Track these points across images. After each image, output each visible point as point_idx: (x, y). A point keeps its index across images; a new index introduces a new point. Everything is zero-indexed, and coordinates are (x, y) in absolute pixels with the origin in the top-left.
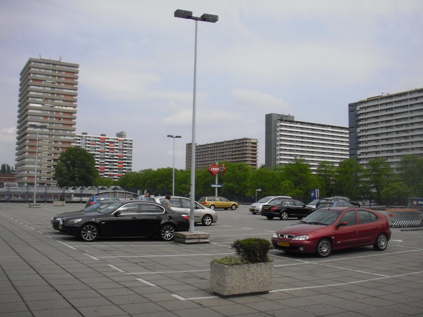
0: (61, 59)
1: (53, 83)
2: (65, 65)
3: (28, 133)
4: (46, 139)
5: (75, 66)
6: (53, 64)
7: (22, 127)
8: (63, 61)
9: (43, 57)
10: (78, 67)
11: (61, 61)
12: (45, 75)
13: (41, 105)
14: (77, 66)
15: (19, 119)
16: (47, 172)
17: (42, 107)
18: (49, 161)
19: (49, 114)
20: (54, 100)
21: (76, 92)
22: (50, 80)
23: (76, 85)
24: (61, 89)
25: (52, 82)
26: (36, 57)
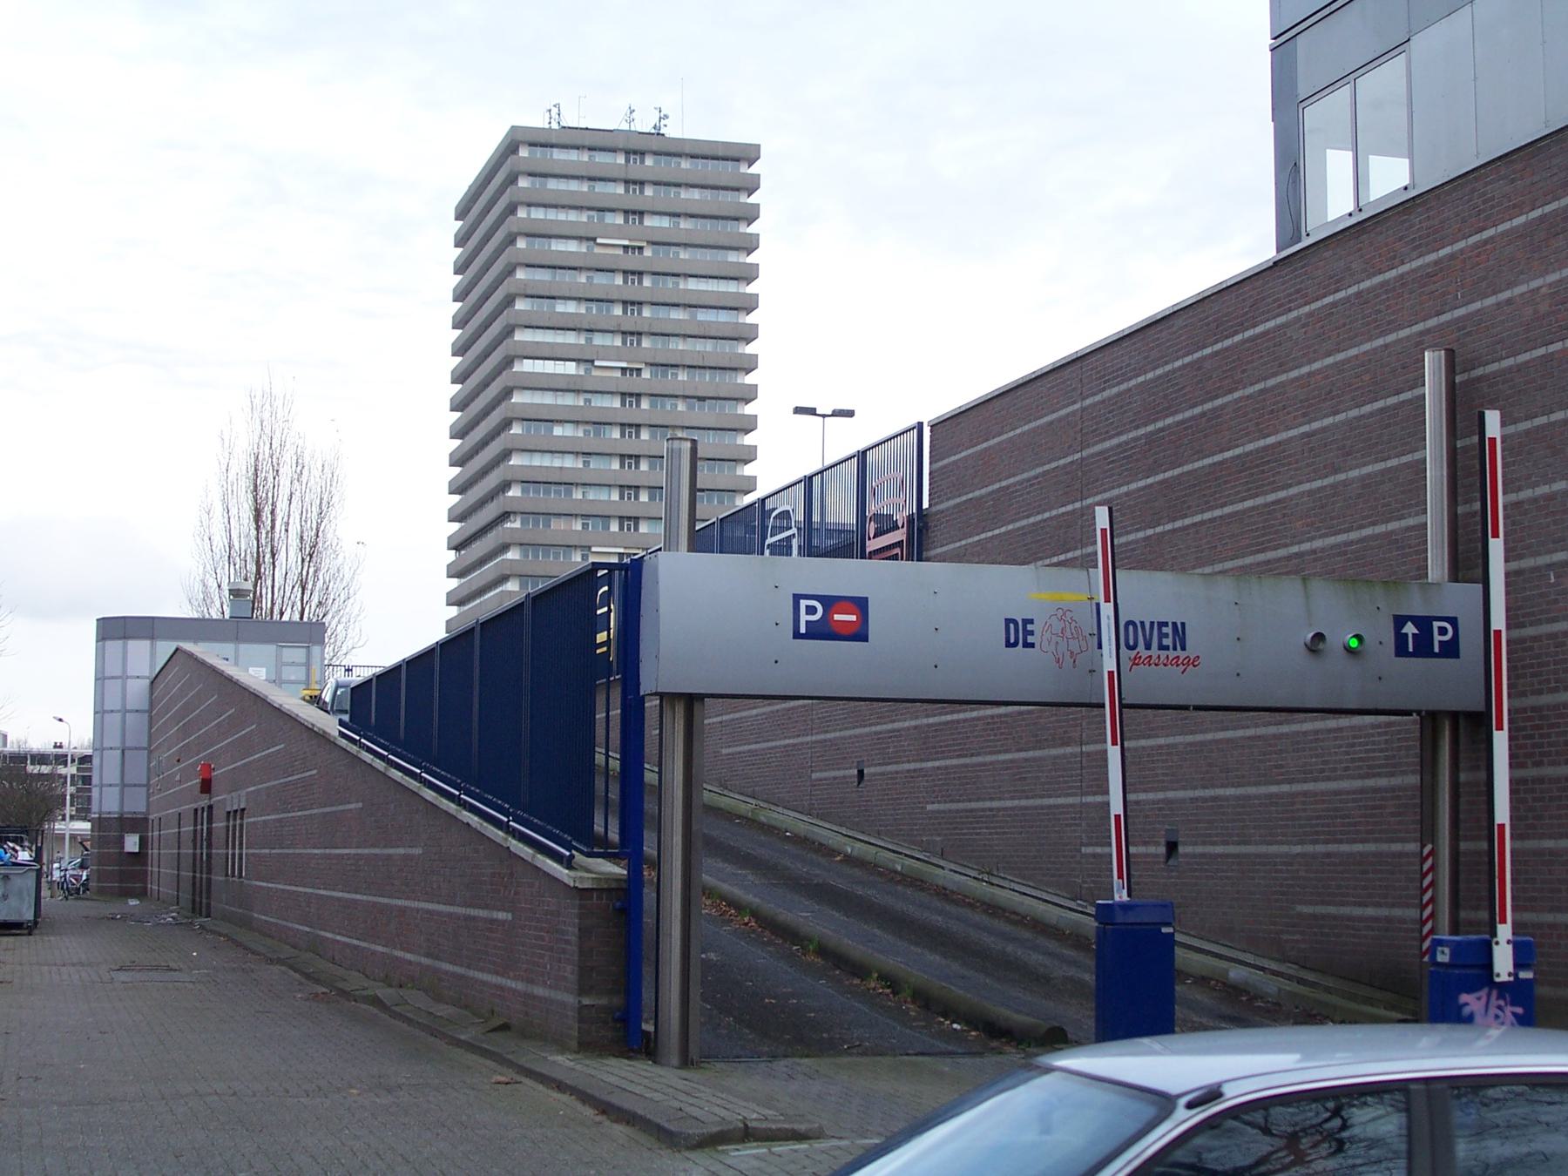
0: (663, 122)
1: (633, 248)
2: (687, 152)
3: (515, 513)
4: (607, 353)
5: (739, 214)
6: (628, 152)
7: (477, 453)
8: (672, 131)
9: (571, 120)
10: (757, 188)
11: (661, 132)
12: (590, 209)
13: (574, 364)
14: (749, 154)
15: (459, 304)
16: (619, 554)
17: (582, 373)
18: (631, 375)
19: (618, 316)
20: (641, 213)
21: (751, 259)
22: (617, 232)
23: (748, 226)
24: (675, 279)
25: (626, 243)
26: (536, 119)
